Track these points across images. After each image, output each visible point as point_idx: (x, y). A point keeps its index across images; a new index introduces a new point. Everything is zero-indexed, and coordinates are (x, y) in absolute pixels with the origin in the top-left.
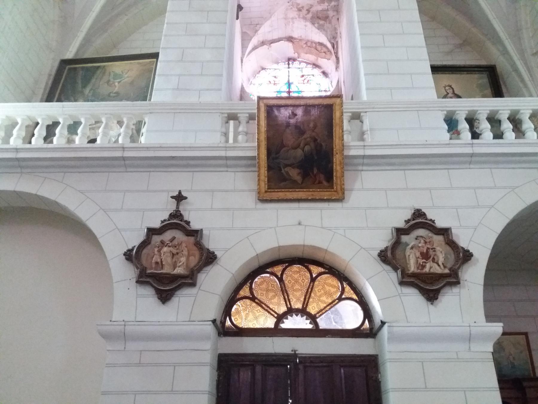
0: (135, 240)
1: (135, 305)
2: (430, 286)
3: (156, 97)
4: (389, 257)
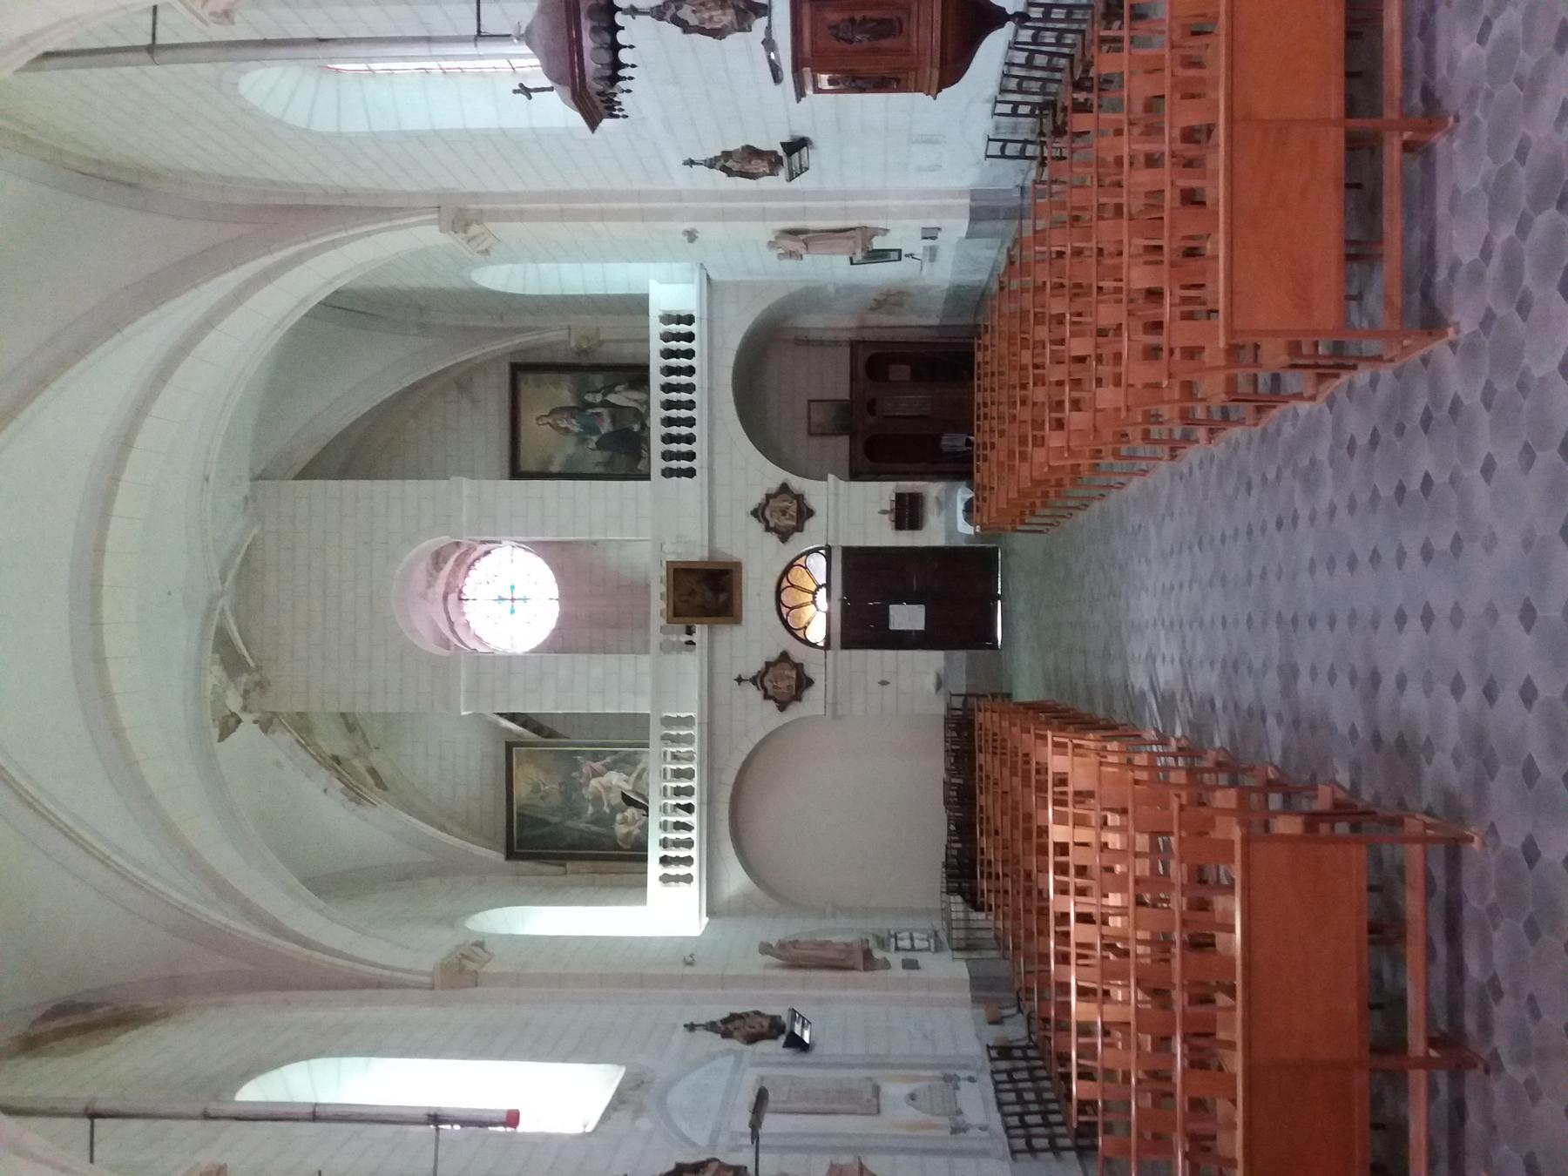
0: (771, 706)
1: (812, 704)
2: (805, 513)
3: (645, 709)
4: (784, 536)
